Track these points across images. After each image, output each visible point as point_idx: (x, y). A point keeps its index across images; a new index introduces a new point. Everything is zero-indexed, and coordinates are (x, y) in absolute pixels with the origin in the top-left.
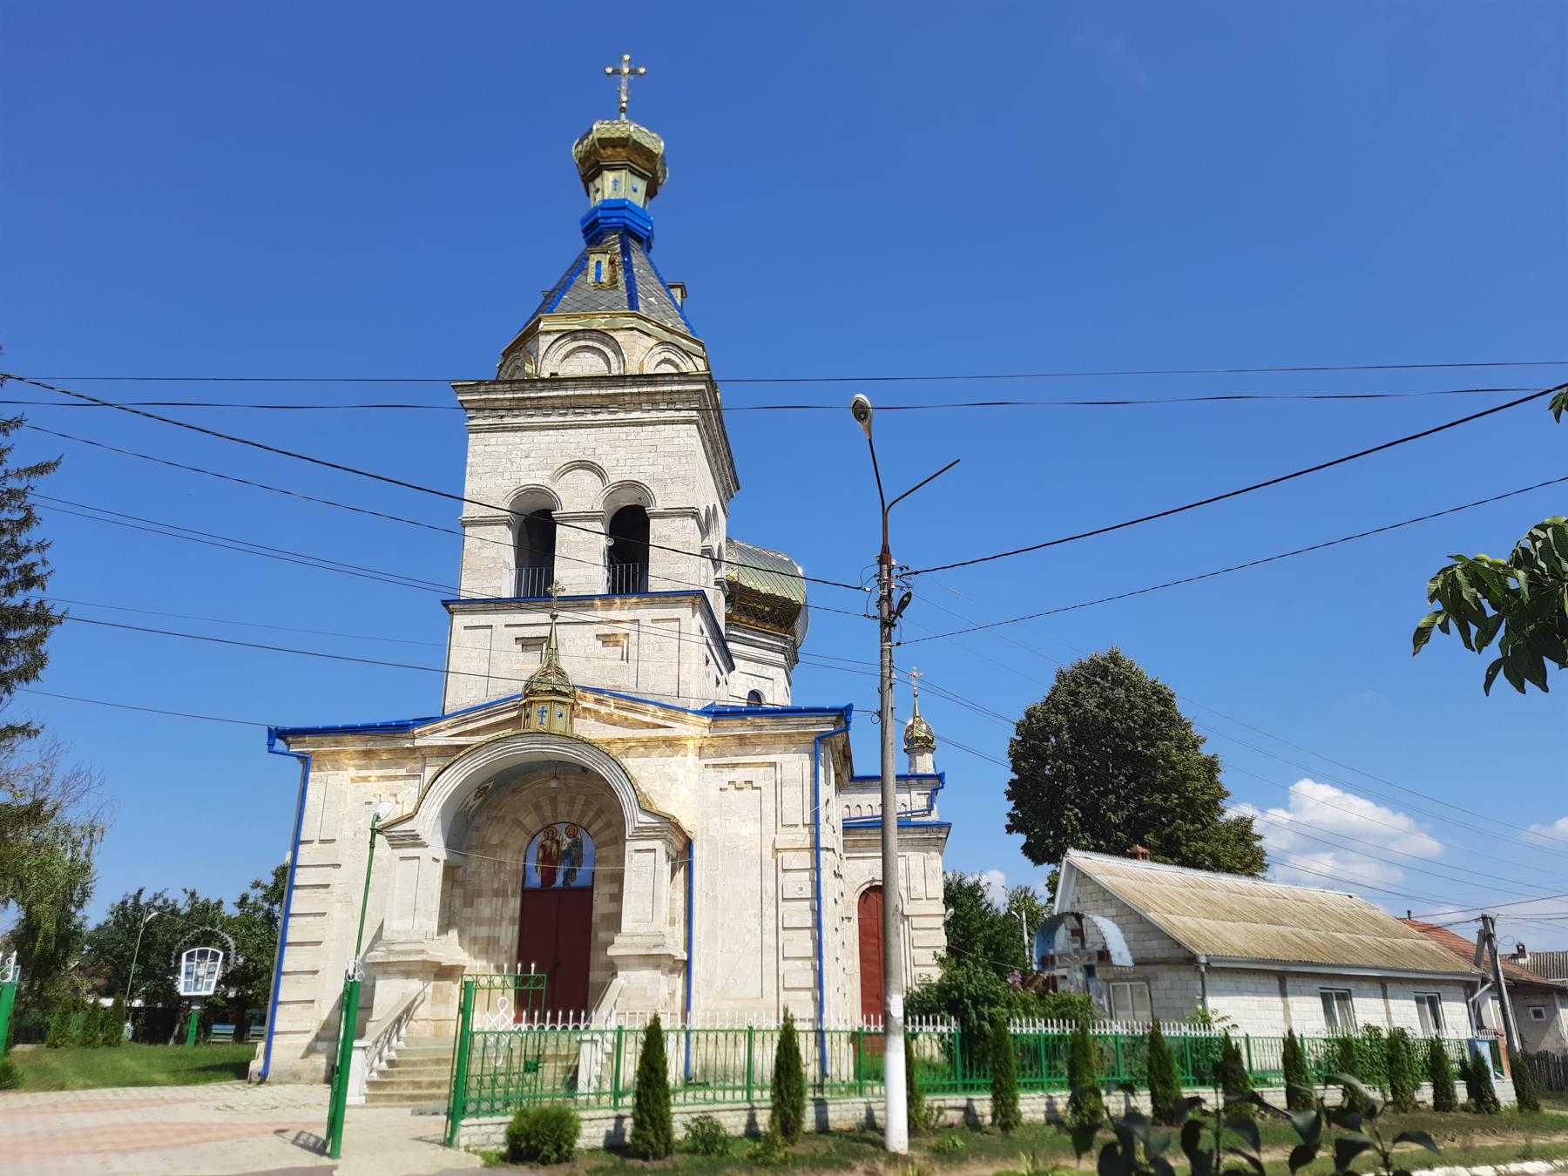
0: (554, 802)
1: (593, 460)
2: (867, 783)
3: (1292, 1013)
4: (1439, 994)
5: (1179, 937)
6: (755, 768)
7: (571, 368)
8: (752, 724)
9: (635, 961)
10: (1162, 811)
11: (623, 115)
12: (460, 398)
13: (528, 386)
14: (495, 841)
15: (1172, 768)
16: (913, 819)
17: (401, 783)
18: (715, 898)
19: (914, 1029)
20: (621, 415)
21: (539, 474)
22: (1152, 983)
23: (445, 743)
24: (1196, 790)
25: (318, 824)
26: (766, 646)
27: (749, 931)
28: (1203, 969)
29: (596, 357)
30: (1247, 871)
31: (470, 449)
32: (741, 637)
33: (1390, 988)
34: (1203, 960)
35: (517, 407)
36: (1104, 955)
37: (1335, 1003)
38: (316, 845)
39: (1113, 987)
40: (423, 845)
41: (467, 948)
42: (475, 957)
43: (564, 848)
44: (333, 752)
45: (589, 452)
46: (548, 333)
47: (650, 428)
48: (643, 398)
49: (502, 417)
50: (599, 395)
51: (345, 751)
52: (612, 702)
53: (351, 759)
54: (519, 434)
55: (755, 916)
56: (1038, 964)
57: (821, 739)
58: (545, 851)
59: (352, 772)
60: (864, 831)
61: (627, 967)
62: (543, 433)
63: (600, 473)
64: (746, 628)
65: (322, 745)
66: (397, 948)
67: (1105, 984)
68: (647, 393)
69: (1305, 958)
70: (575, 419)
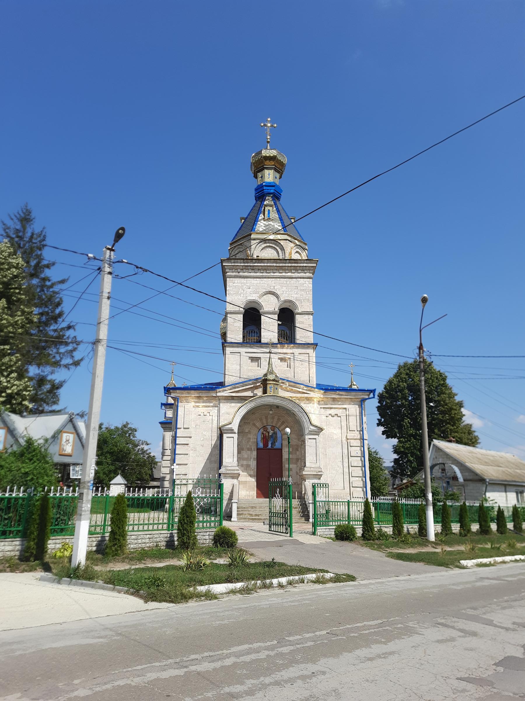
0: (266, 418)
5: (478, 472)
6: (338, 409)
7: (264, 254)
10: (442, 421)
15: (446, 405)
17: (211, 408)
20: (284, 274)
21: (254, 295)
22: (466, 488)
23: (228, 395)
24: (455, 414)
25: (183, 422)
27: (338, 466)
28: (487, 483)
29: (273, 250)
30: (473, 445)
34: (488, 480)
36: (455, 478)
38: (182, 429)
43: (270, 434)
45: (272, 288)
46: (254, 239)
47: (295, 280)
48: (292, 268)
52: (287, 383)
53: (192, 399)
54: (246, 279)
58: (264, 435)
59: (193, 404)
62: (255, 279)
63: (277, 297)
65: (183, 394)
66: (229, 468)
68: (294, 266)
69: (513, 479)
70: (266, 274)
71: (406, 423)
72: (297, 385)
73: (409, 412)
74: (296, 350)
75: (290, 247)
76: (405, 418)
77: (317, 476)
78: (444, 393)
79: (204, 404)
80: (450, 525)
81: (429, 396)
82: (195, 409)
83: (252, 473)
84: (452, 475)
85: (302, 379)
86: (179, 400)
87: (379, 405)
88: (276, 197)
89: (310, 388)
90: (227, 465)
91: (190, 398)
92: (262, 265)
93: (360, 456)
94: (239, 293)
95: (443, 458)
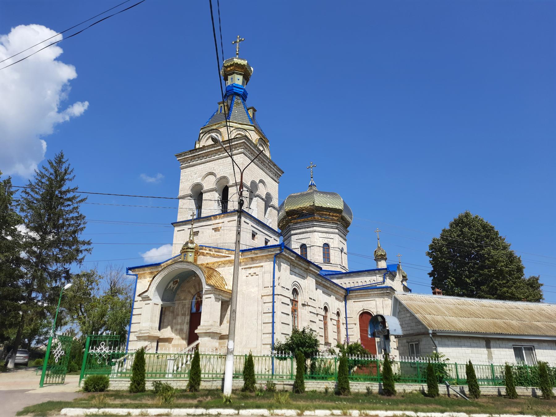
1: (213, 172)
3: (493, 355)
4: (533, 346)
7: (208, 143)
8: (254, 253)
9: (203, 335)
11: (237, 56)
12: (178, 159)
13: (195, 151)
14: (183, 298)
15: (492, 258)
16: (377, 286)
18: (243, 313)
19: (285, 356)
21: (199, 179)
26: (329, 227)
27: (253, 324)
28: (431, 335)
31: (181, 174)
32: (319, 225)
33: (492, 343)
34: (431, 332)
35: (193, 158)
37: (524, 352)
39: (410, 345)
40: (150, 300)
41: (174, 332)
42: (176, 335)
44: (143, 273)
45: (212, 169)
49: (189, 163)
50: (215, 150)
51: (146, 273)
53: (148, 275)
54: (194, 167)
55: (255, 319)
56: (371, 335)
57: (276, 256)
60: (358, 291)
61: (202, 337)
64: (321, 221)
66: (143, 332)
67: (407, 343)
74: (226, 219)
78: (487, 245)
83: (184, 336)
88: (244, 97)
92: (204, 152)
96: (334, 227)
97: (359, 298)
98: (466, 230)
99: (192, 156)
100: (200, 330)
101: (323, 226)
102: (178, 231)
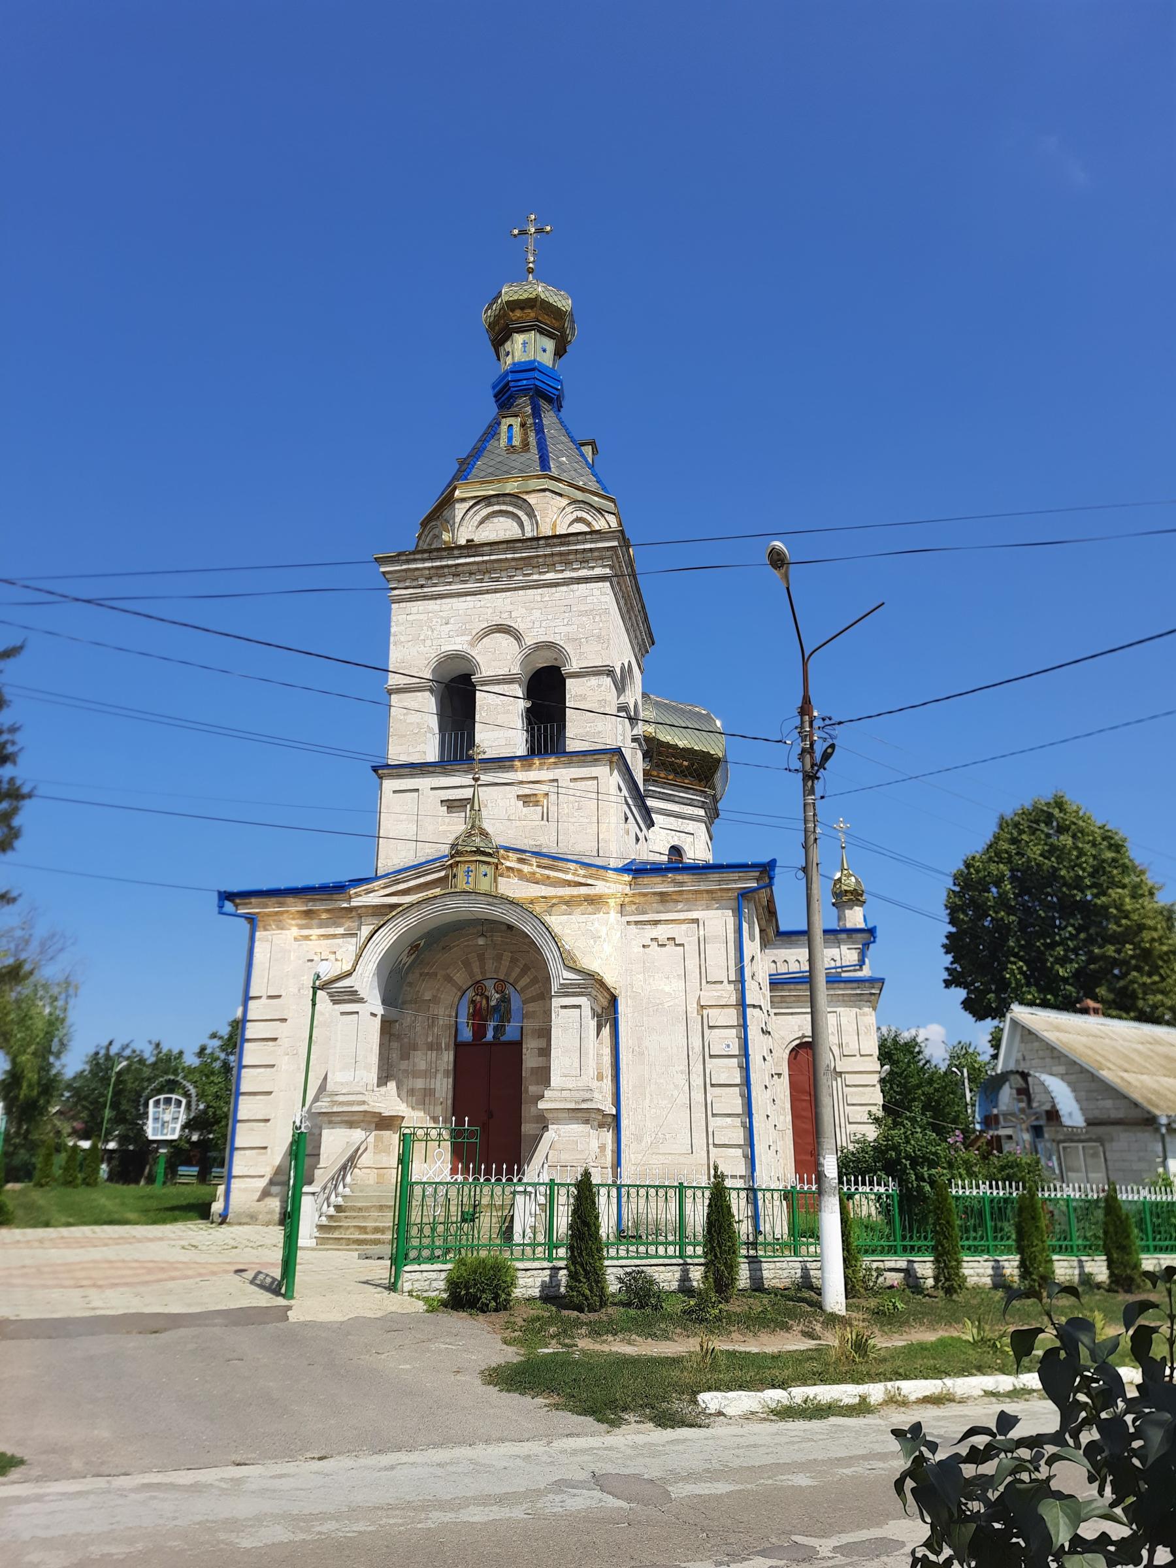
1: (509, 624)
2: (794, 938)
5: (1136, 1096)
7: (486, 533)
12: (382, 569)
13: (445, 553)
14: (427, 996)
15: (1126, 917)
16: (843, 975)
21: (458, 640)
22: (1108, 1146)
24: (1153, 940)
27: (676, 1086)
28: (1164, 1130)
29: (510, 520)
31: (394, 619)
32: (659, 792)
36: (1053, 1115)
38: (264, 1000)
40: (361, 1001)
42: (413, 1108)
43: (493, 1003)
44: (277, 913)
45: (505, 615)
46: (463, 500)
47: (564, 588)
48: (556, 558)
50: (513, 559)
51: (287, 912)
52: (534, 861)
53: (293, 919)
54: (438, 602)
58: (475, 1007)
59: (295, 931)
60: (792, 987)
61: (557, 1121)
62: (463, 599)
63: (516, 635)
64: (665, 783)
65: (266, 906)
66: (341, 1098)
67: (1054, 1144)
71: (1013, 973)
72: (560, 864)
73: (1023, 942)
75: (555, 509)
76: (1012, 959)
77: (580, 1115)
78: (1114, 884)
79: (322, 931)
80: (959, 1262)
81: (1075, 895)
82: (300, 945)
84: (1047, 1107)
85: (579, 848)
86: (260, 924)
87: (954, 930)
89: (593, 871)
90: (338, 1089)
91: (285, 915)
93: (737, 1053)
94: (422, 638)
95: (1043, 1058)
96: (696, 803)
97: (790, 1005)
98: (1066, 840)
99: (432, 567)
100: (551, 1100)
101: (668, 798)
102: (395, 792)
